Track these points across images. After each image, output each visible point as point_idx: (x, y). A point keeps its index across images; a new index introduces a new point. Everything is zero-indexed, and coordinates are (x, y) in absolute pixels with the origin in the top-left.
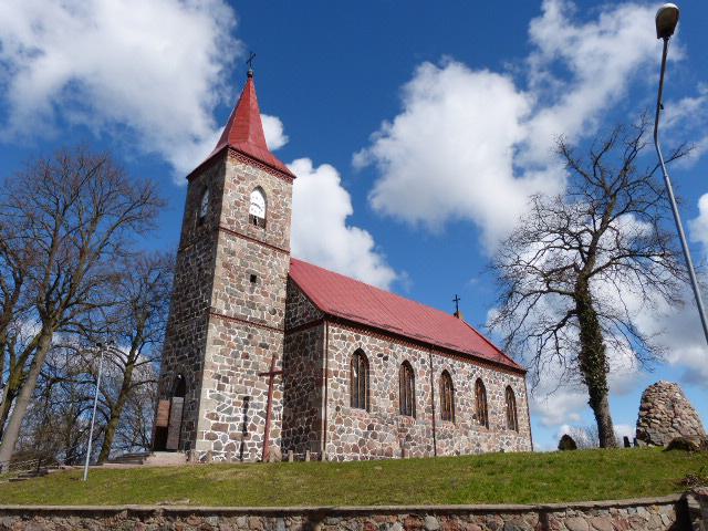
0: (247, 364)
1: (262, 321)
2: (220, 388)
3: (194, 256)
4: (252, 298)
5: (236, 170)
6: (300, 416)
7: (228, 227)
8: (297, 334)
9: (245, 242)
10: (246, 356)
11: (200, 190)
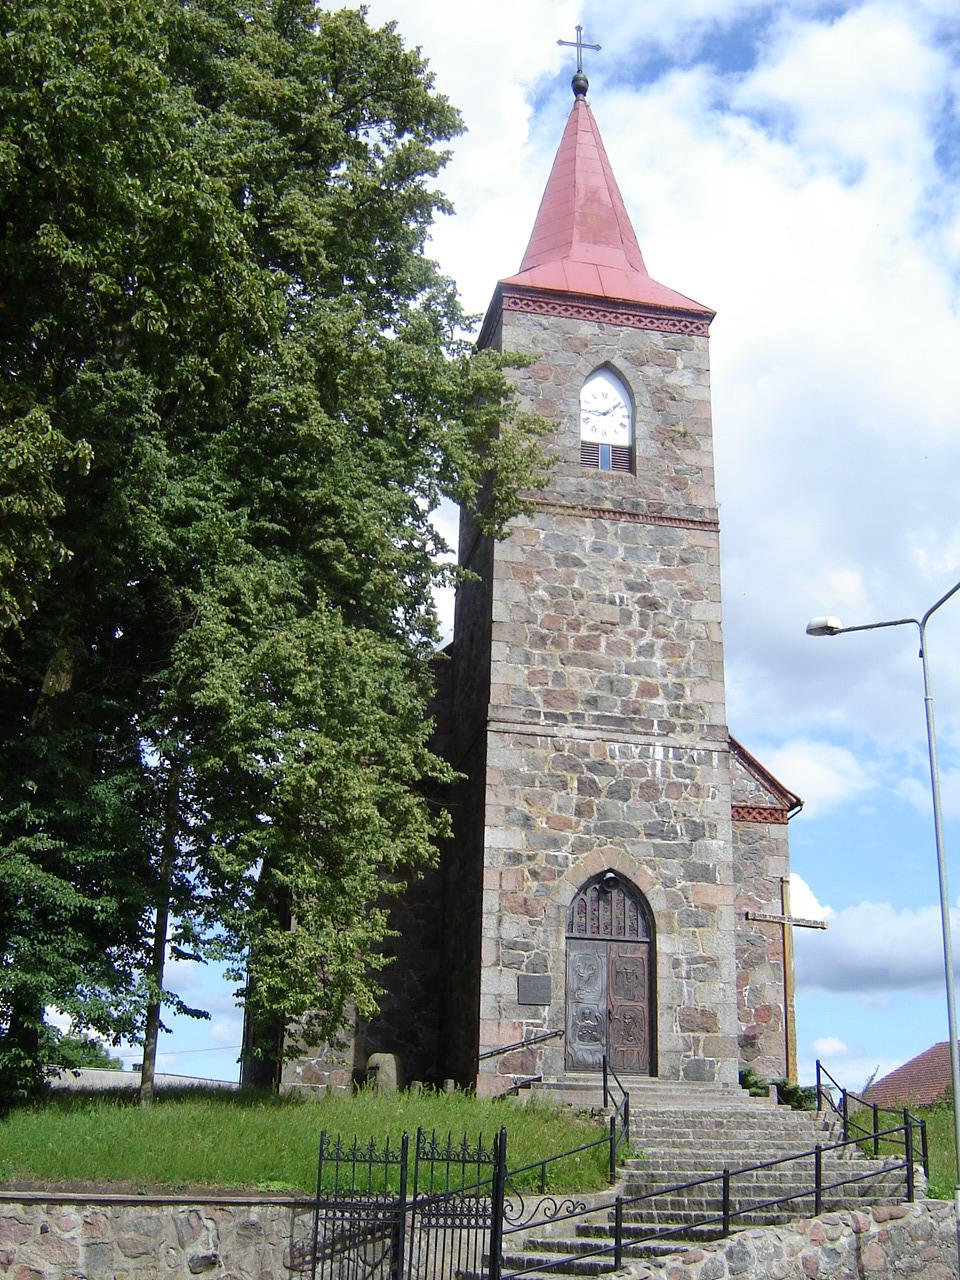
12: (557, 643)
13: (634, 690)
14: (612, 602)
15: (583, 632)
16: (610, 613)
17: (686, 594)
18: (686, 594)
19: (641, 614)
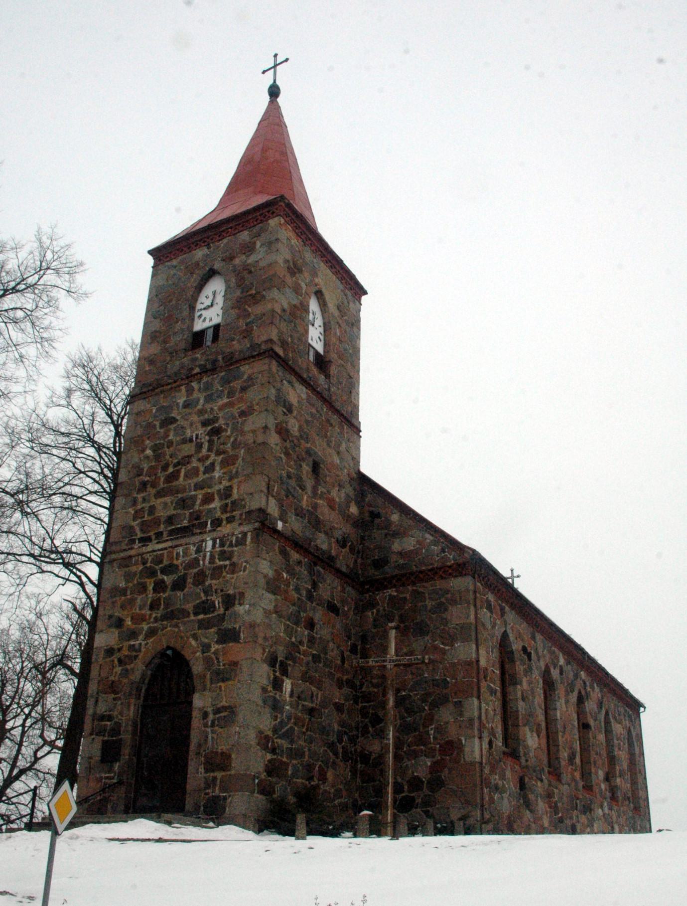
0: (311, 640)
1: (332, 559)
2: (277, 685)
3: (186, 405)
5: (291, 248)
6: (415, 755)
7: (281, 352)
9: (302, 391)
10: (311, 625)
11: (195, 279)
12: (153, 486)
13: (198, 502)
14: (191, 440)
15: (171, 470)
16: (188, 449)
17: (290, 410)
18: (243, 414)
19: (209, 441)
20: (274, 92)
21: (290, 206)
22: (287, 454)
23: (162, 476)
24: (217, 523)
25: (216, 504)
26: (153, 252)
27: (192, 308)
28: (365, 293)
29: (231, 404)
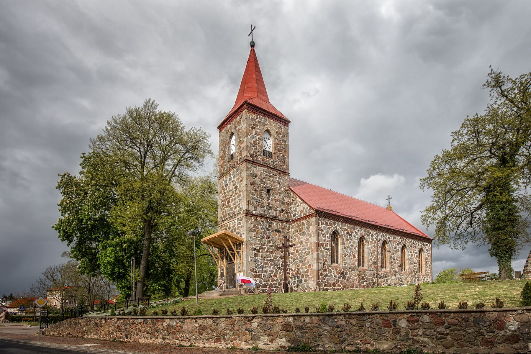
0: (269, 242)
3: (230, 180)
4: (269, 203)
8: (298, 223)
9: (261, 169)
10: (269, 237)
20: (253, 45)
21: (249, 103)
22: (255, 190)
23: (227, 202)
24: (238, 214)
25: (237, 209)
26: (219, 127)
27: (229, 147)
28: (290, 122)
29: (238, 179)
